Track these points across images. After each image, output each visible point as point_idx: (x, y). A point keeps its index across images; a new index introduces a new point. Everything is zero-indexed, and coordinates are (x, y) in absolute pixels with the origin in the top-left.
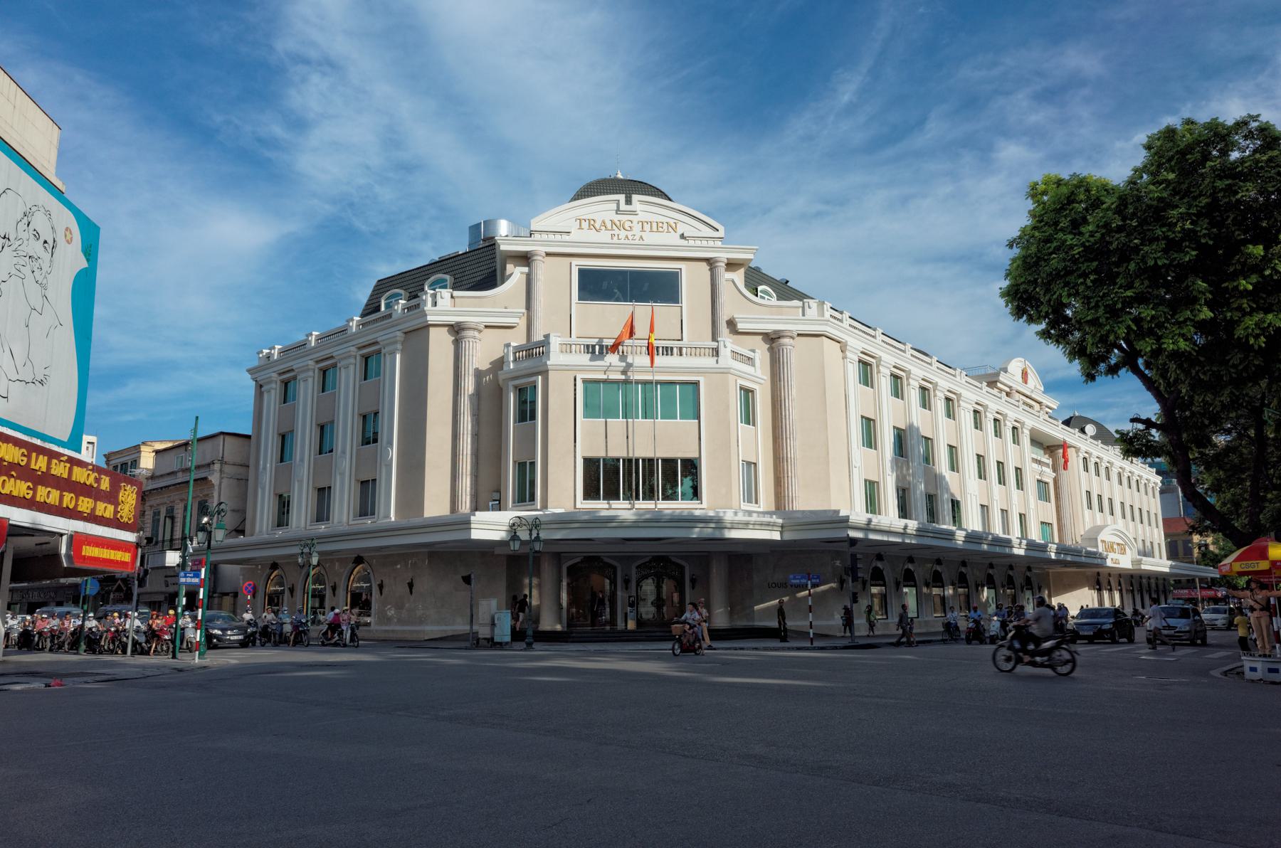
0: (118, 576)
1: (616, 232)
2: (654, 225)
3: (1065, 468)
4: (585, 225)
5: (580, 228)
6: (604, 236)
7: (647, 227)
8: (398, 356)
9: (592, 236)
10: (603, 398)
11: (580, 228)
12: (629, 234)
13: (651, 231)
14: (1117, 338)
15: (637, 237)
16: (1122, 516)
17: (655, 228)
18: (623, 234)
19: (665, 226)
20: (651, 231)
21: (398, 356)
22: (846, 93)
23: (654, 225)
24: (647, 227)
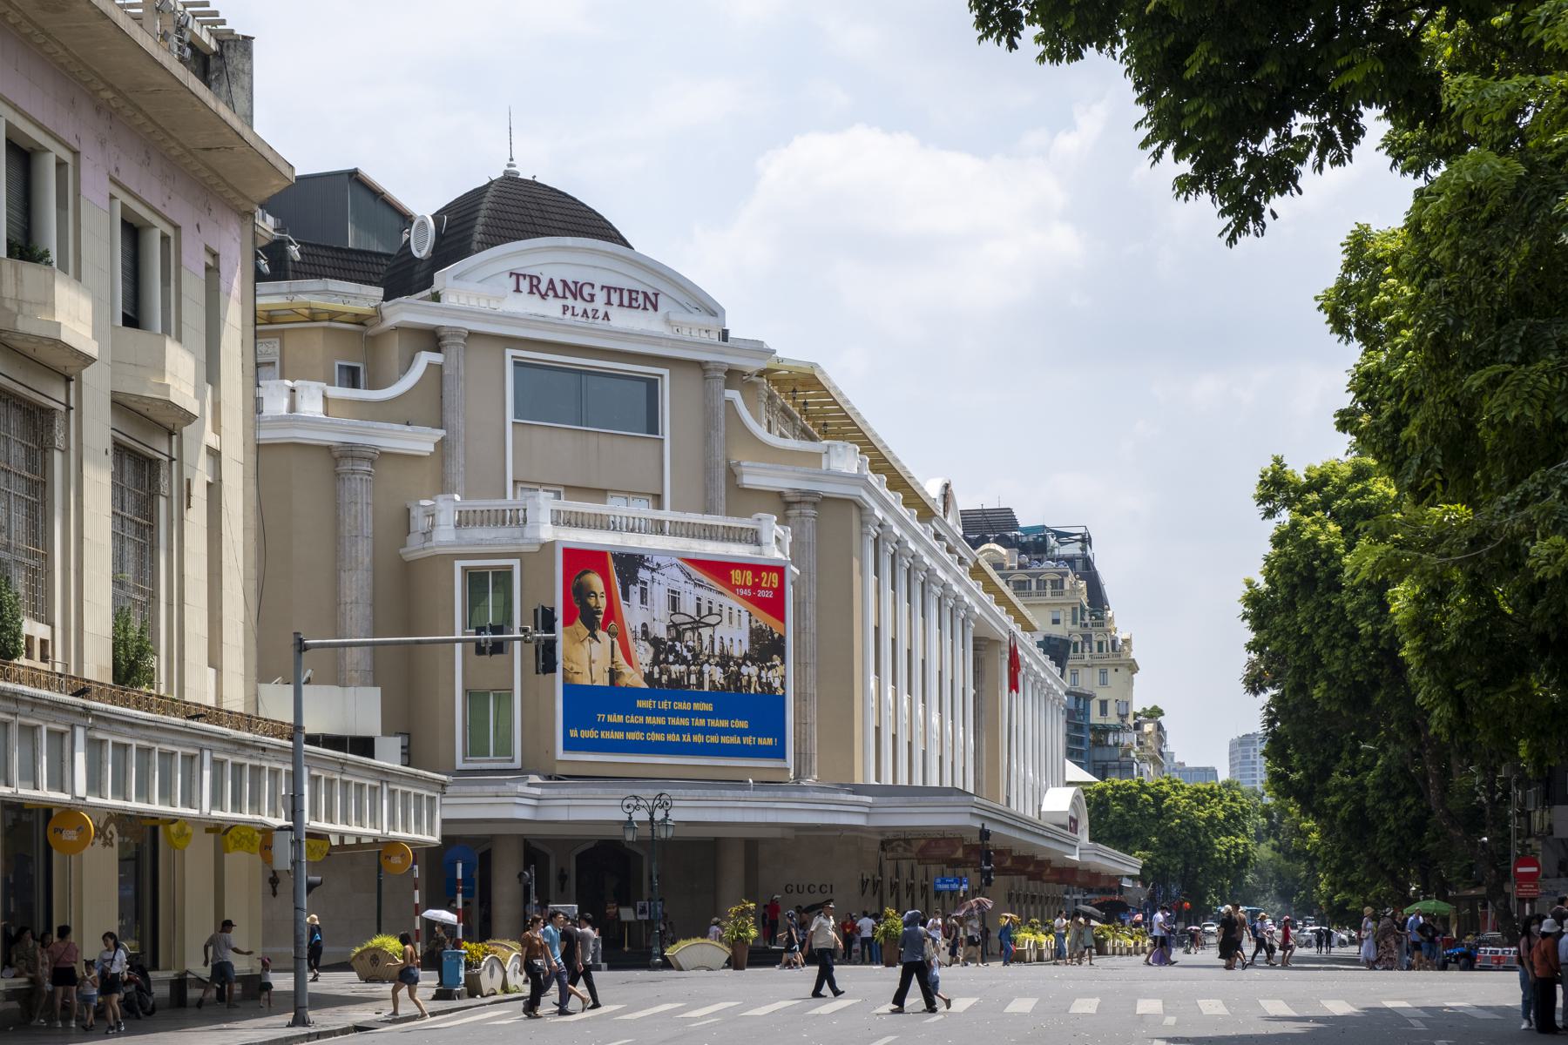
1: (570, 302)
2: (626, 295)
3: (189, 506)
4: (525, 285)
5: (518, 290)
6: (552, 308)
7: (615, 298)
8: (460, 876)
9: (526, 305)
11: (518, 290)
12: (589, 307)
13: (621, 305)
15: (601, 314)
16: (1008, 1010)
17: (626, 302)
18: (580, 306)
19: (641, 298)
20: (621, 305)
21: (460, 876)
22: (1406, 581)
23: (626, 295)
24: (615, 298)
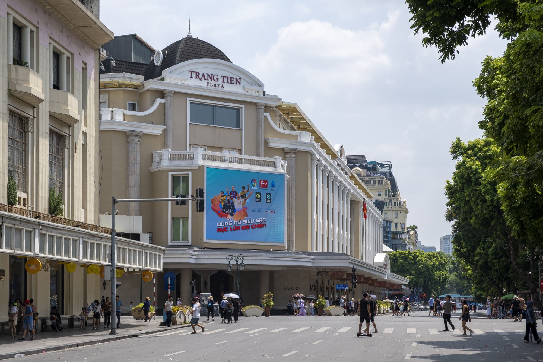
0: (219, 319)
1: (210, 81)
2: (229, 79)
4: (194, 75)
5: (191, 77)
7: (226, 80)
8: (169, 283)
10: (99, 245)
11: (191, 77)
12: (217, 83)
13: (228, 82)
14: (515, 192)
15: (220, 86)
17: (229, 81)
18: (213, 83)
19: (235, 80)
20: (228, 82)
21: (169, 283)
23: (229, 79)
24: (226, 80)
